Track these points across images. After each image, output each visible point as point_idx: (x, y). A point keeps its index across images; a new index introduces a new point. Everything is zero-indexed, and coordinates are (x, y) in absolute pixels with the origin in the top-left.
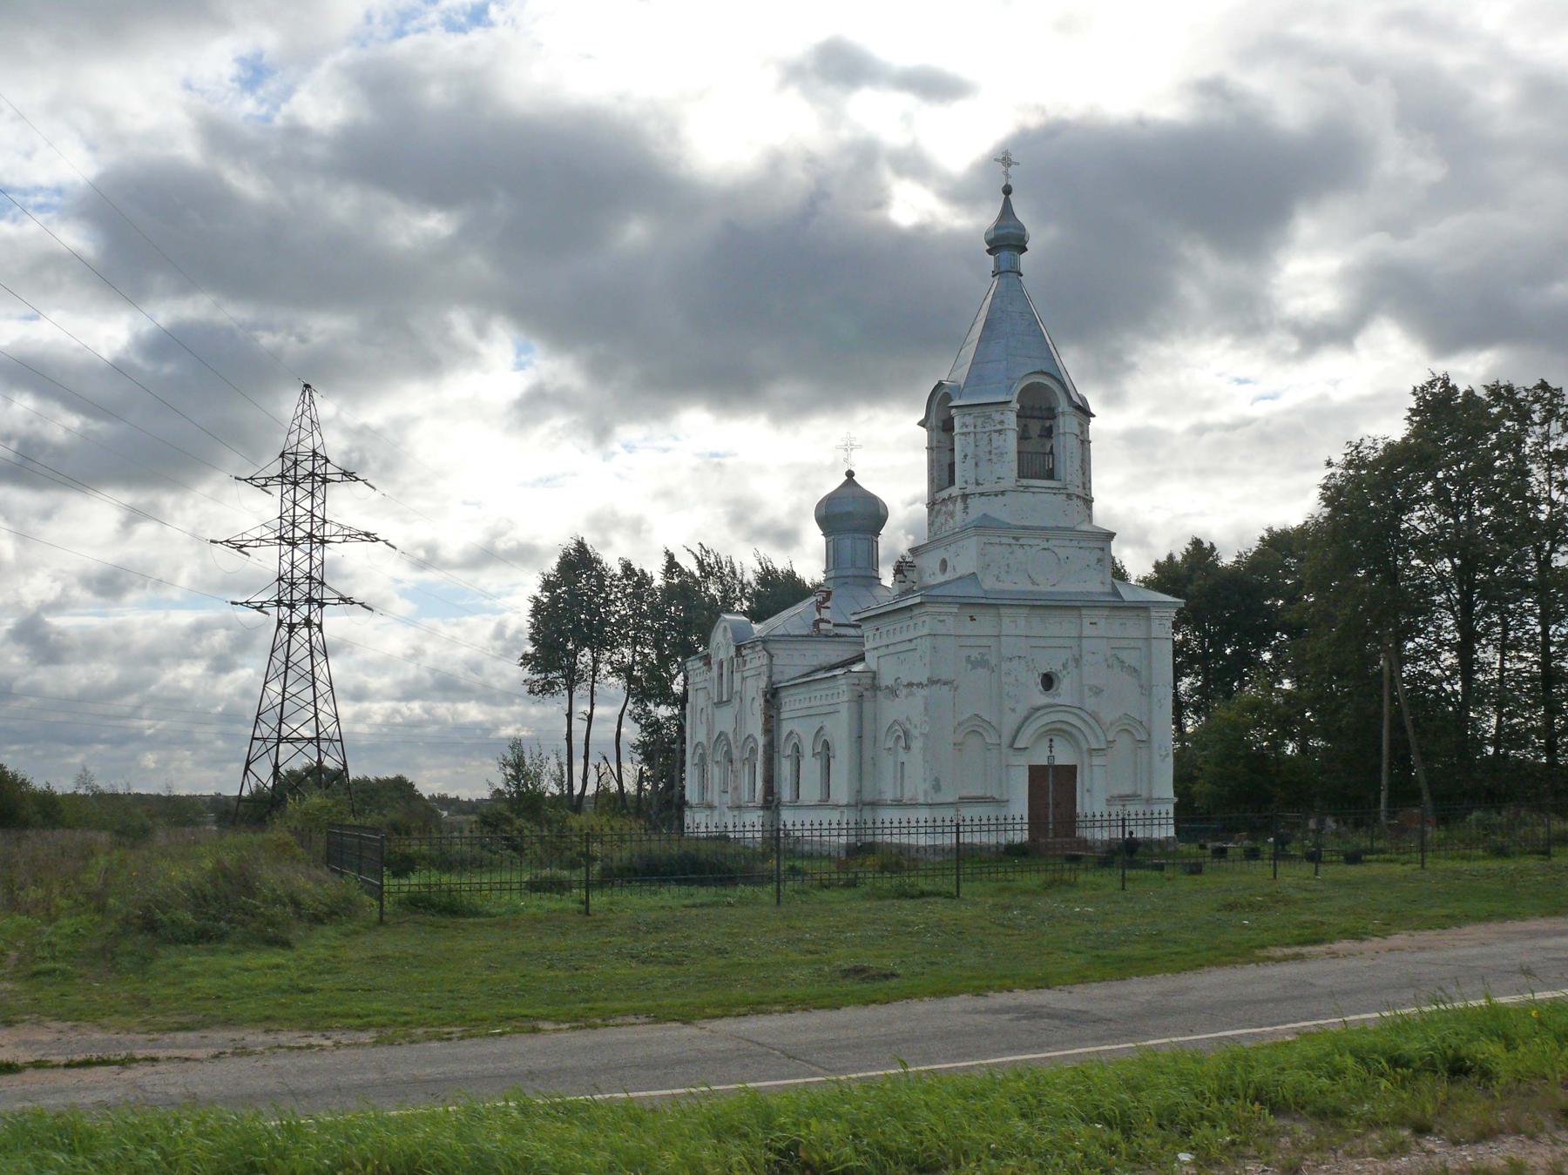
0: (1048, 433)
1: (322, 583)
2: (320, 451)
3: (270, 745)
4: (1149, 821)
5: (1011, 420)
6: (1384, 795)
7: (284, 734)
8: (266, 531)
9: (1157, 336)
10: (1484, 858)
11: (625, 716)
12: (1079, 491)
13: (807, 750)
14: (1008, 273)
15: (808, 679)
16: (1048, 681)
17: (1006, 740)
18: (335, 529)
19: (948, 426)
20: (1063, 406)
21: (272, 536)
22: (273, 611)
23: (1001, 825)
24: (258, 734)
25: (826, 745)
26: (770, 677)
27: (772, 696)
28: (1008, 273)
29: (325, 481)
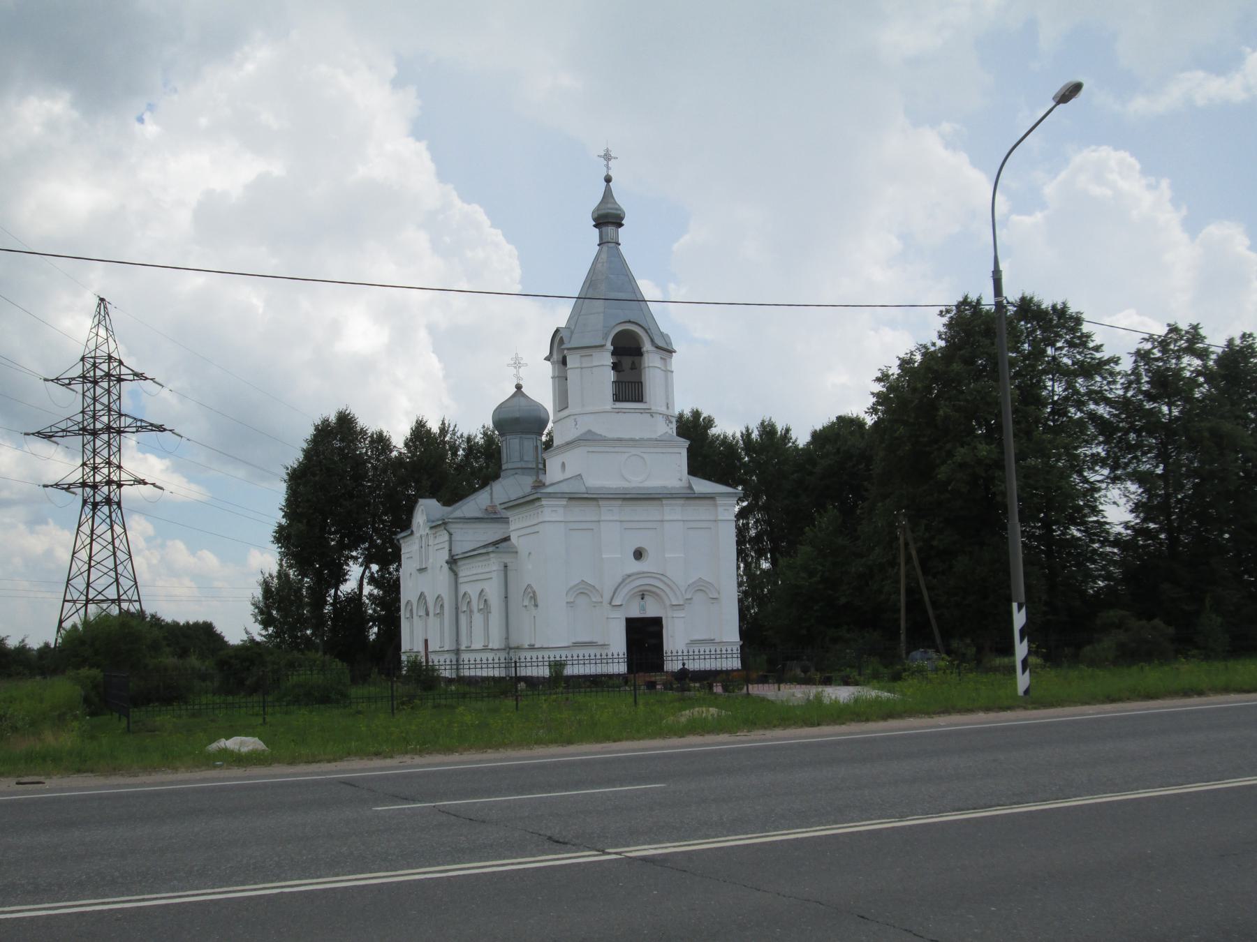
1: (119, 467)
2: (115, 355)
3: (79, 606)
5: (608, 360)
6: (903, 637)
7: (90, 597)
8: (70, 423)
11: (365, 581)
12: (663, 409)
15: (470, 556)
16: (638, 554)
17: (607, 596)
18: (129, 421)
20: (647, 346)
21: (76, 428)
22: (79, 491)
24: (69, 597)
27: (453, 562)
29: (120, 380)
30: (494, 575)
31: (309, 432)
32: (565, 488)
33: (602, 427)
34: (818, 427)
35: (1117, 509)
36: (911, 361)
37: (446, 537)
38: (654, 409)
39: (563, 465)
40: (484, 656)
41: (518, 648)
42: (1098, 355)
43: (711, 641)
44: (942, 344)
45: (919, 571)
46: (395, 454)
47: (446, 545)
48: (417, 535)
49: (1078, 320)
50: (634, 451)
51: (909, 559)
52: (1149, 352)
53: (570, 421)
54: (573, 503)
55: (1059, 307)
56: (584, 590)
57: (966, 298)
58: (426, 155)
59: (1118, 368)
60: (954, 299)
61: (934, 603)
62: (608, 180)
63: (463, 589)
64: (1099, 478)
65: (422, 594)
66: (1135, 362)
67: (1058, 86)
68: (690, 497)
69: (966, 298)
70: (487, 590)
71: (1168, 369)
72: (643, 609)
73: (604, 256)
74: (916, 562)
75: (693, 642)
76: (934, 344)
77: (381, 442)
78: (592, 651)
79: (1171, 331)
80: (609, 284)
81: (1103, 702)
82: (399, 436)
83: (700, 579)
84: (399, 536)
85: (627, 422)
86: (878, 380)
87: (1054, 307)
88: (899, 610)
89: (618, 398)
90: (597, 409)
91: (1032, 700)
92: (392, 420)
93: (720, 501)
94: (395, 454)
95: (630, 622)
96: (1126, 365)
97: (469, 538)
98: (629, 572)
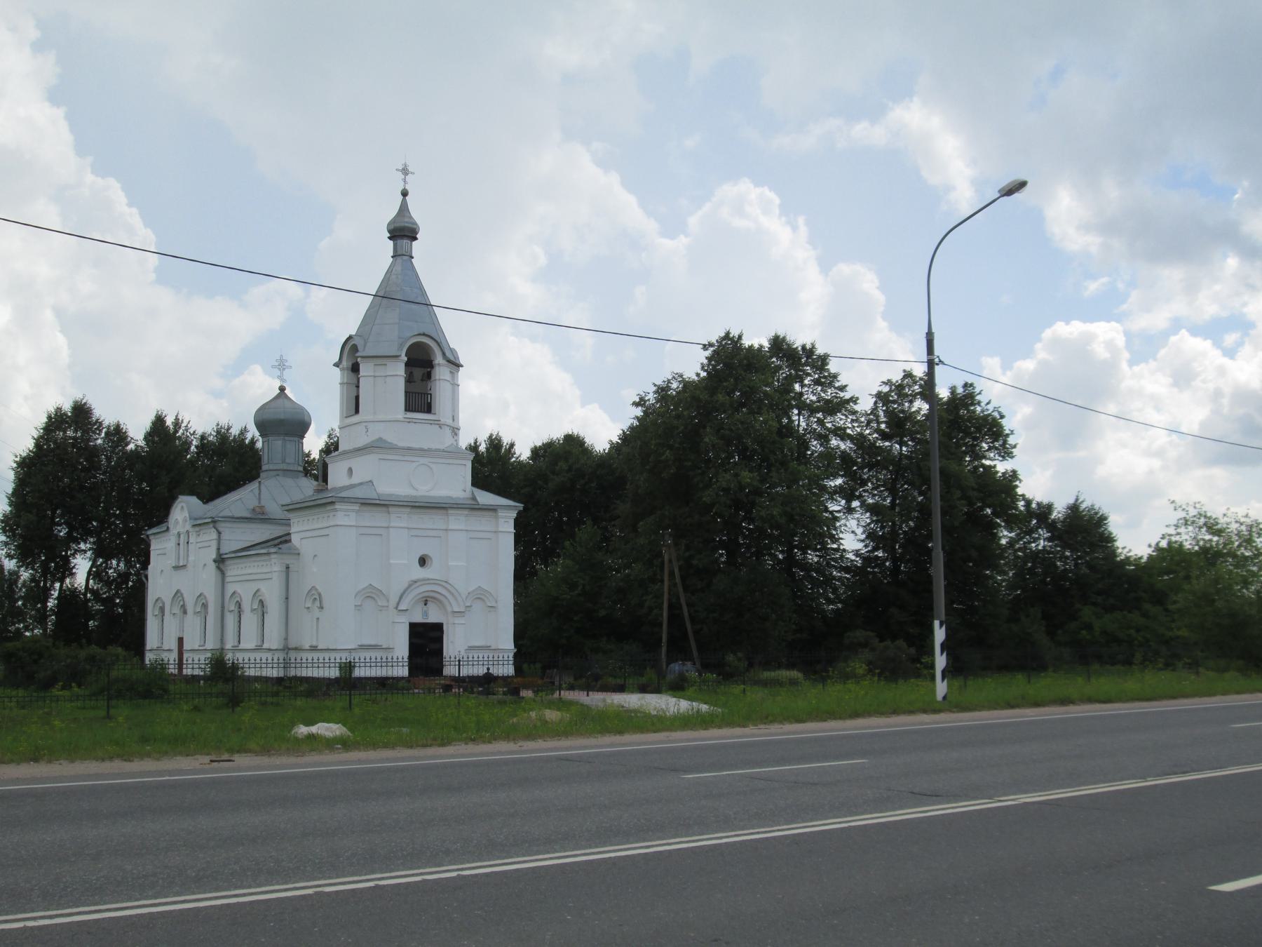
0: (428, 376)
4: (496, 662)
6: (664, 649)
9: (181, 754)
10: (344, 744)
12: (449, 422)
13: (246, 606)
14: (402, 256)
15: (245, 552)
16: (423, 561)
19: (355, 369)
20: (439, 359)
23: (388, 663)
25: (261, 602)
26: (218, 549)
27: (220, 561)
28: (402, 256)
30: (275, 576)
31: (42, 420)
32: (358, 493)
33: (393, 436)
34: (539, 444)
35: (852, 537)
36: (668, 388)
37: (214, 535)
38: (443, 421)
39: (350, 470)
40: (258, 655)
41: (296, 649)
42: (842, 394)
43: (487, 648)
44: (703, 374)
45: (681, 589)
46: (131, 446)
47: (214, 545)
48: (174, 531)
49: (824, 359)
50: (423, 460)
51: (672, 574)
52: (887, 395)
53: (361, 428)
54: (365, 508)
55: (808, 347)
56: (371, 594)
57: (728, 334)
58: (63, 126)
59: (857, 408)
60: (714, 336)
61: (692, 619)
62: (405, 194)
63: (230, 589)
64: (838, 508)
65: (178, 591)
66: (876, 403)
67: (1006, 181)
68: (474, 508)
69: (728, 334)
70: (263, 590)
71: (903, 411)
72: (426, 614)
73: (398, 268)
74: (678, 580)
75: (471, 648)
76: (698, 375)
77: (118, 435)
78: (378, 654)
79: (905, 377)
80: (400, 294)
81: (1003, 708)
82: (137, 432)
83: (477, 588)
84: (149, 532)
85: (417, 431)
86: (636, 404)
87: (804, 347)
88: (661, 625)
89: (409, 408)
90: (389, 417)
91: (949, 705)
92: (129, 413)
93: (501, 513)
94: (131, 446)
95: (413, 626)
96: (865, 404)
97: (237, 537)
98: (414, 578)
